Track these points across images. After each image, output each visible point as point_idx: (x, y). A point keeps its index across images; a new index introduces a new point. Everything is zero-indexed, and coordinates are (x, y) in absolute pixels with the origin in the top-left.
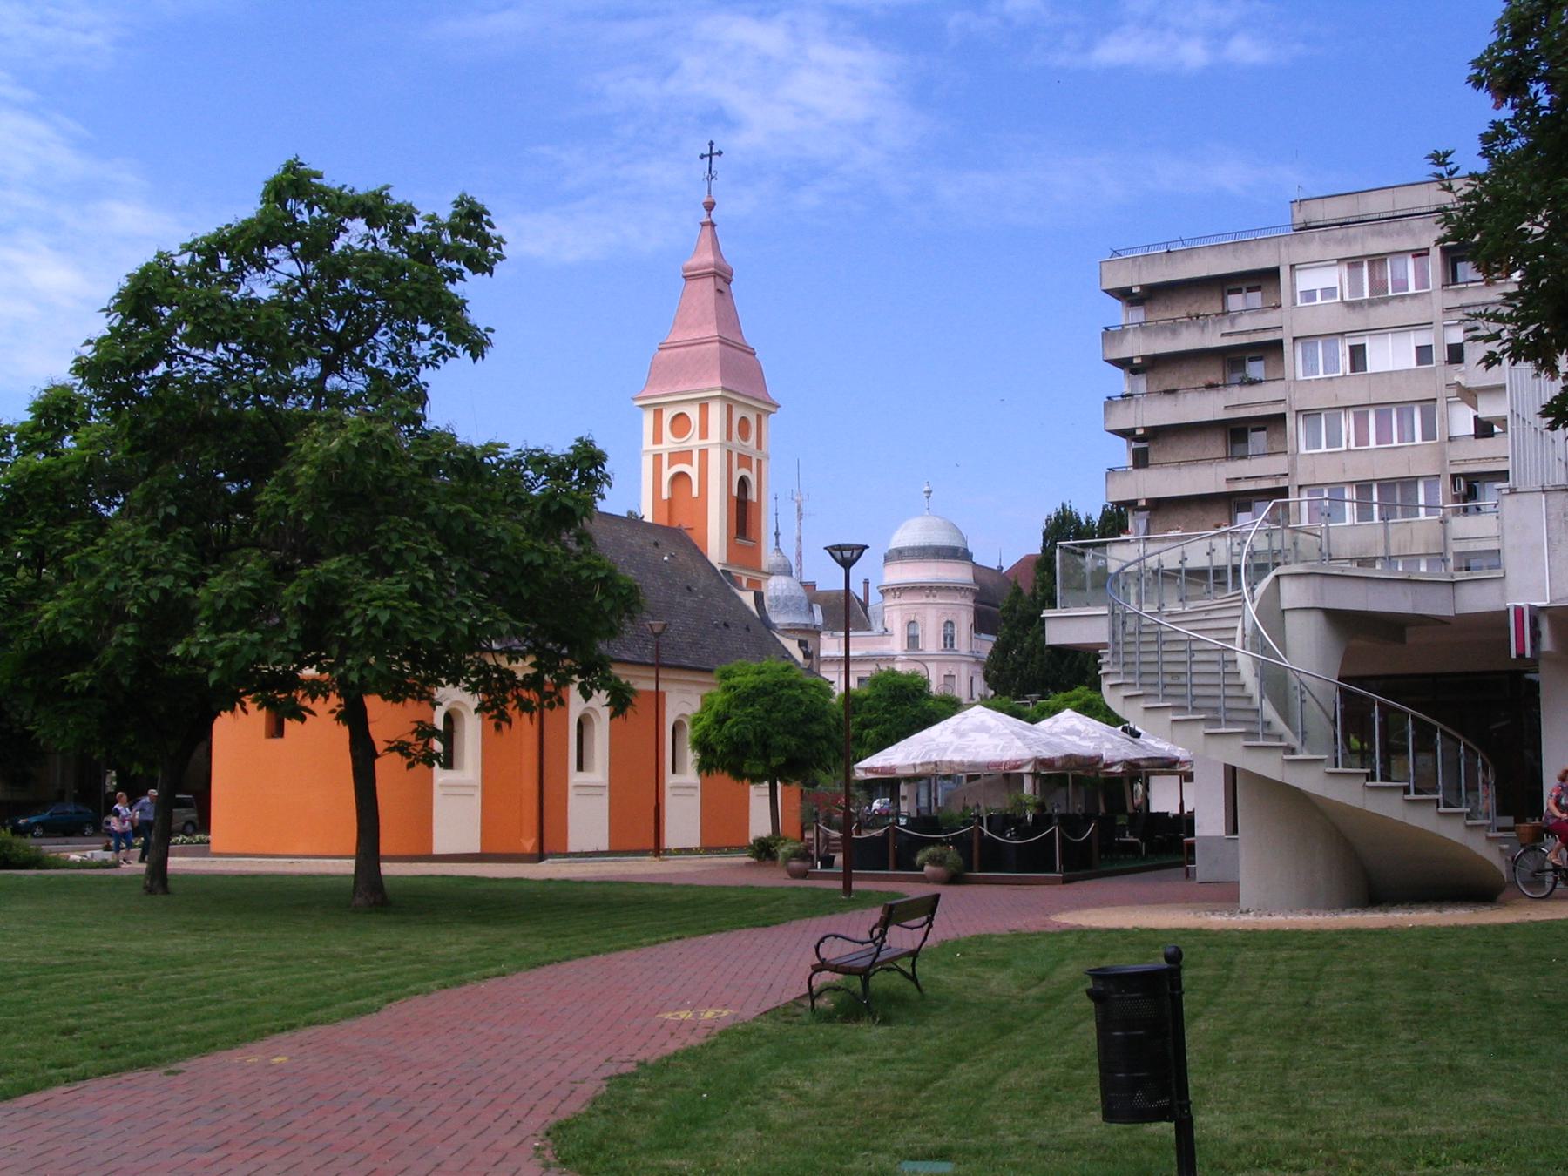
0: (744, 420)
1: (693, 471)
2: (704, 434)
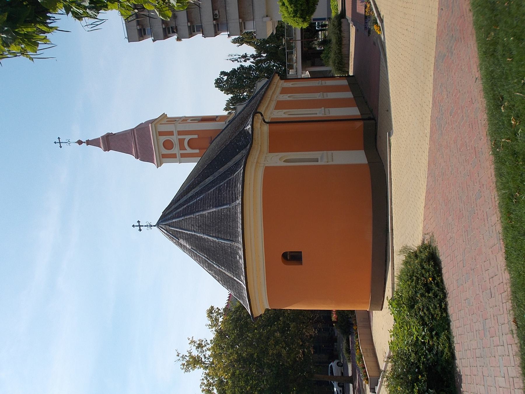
0: (167, 121)
1: (188, 138)
2: (171, 133)
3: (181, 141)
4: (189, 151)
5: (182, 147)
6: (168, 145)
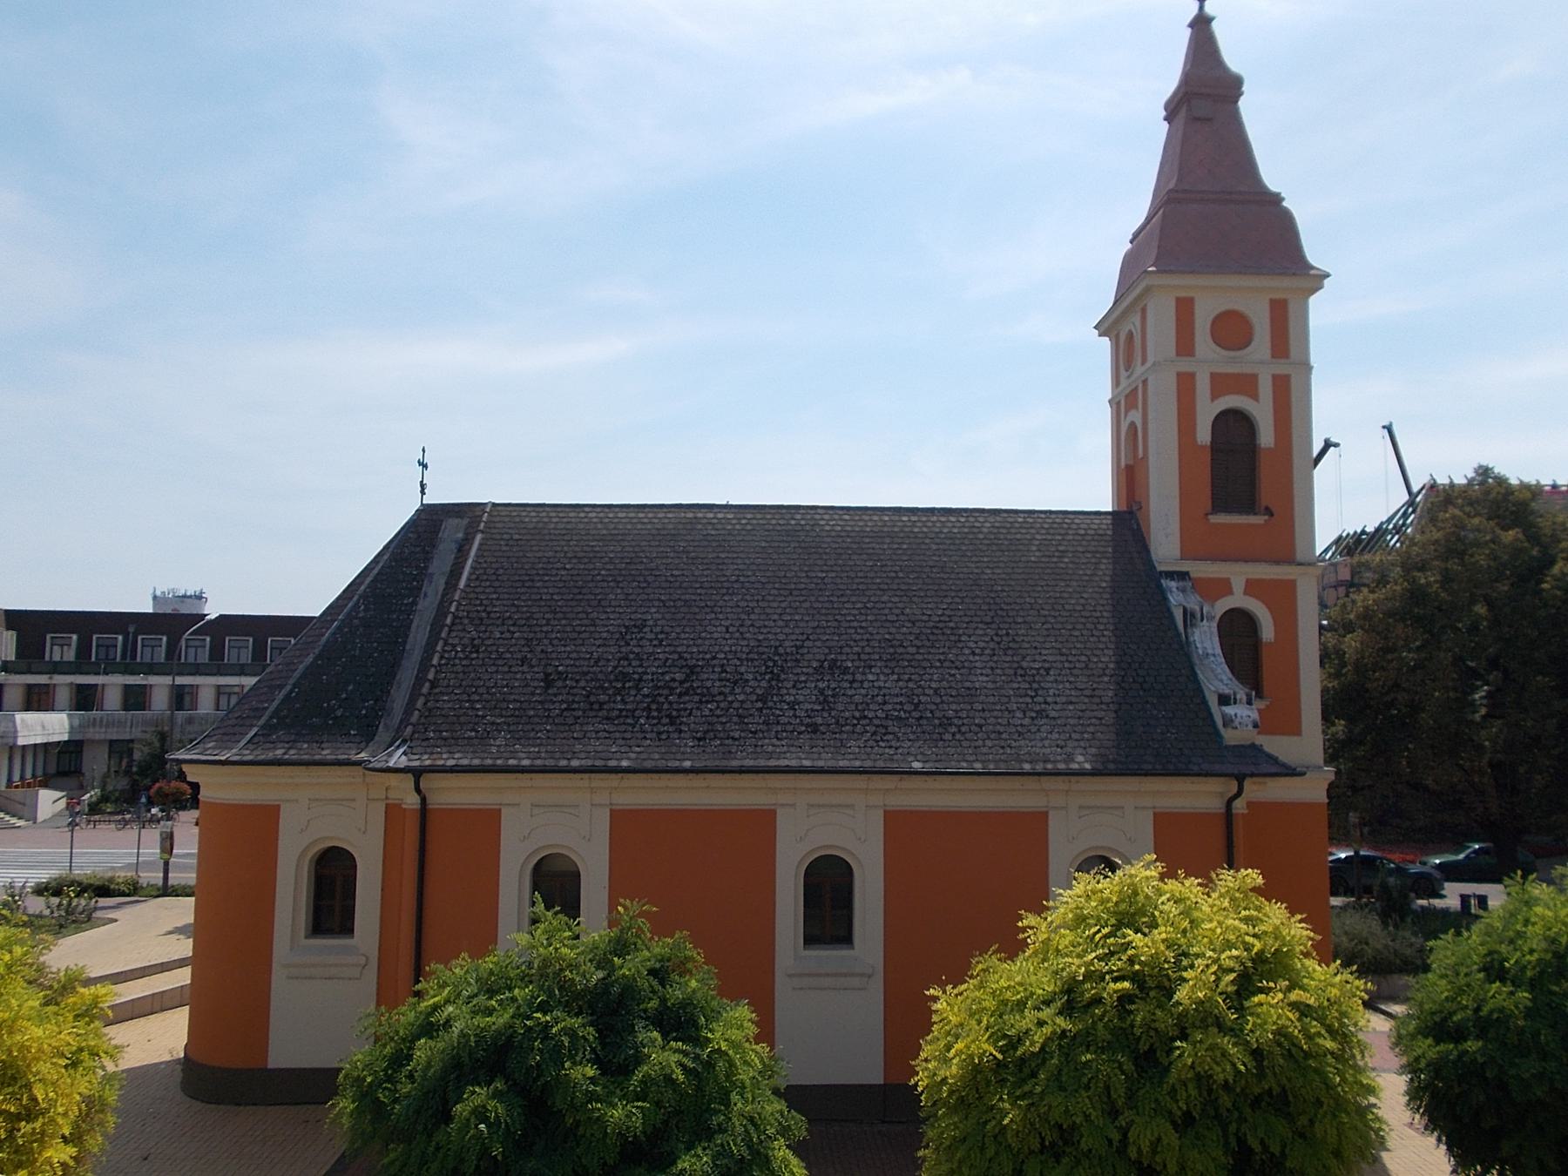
1: (1262, 412)
3: (1247, 384)
4: (1207, 412)
5: (1221, 384)
6: (1232, 331)
